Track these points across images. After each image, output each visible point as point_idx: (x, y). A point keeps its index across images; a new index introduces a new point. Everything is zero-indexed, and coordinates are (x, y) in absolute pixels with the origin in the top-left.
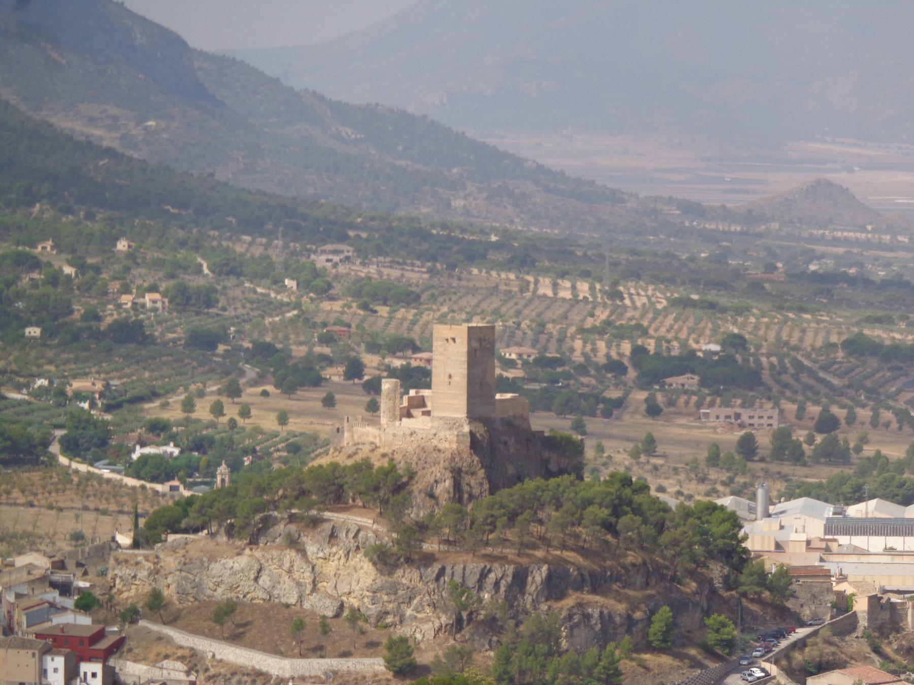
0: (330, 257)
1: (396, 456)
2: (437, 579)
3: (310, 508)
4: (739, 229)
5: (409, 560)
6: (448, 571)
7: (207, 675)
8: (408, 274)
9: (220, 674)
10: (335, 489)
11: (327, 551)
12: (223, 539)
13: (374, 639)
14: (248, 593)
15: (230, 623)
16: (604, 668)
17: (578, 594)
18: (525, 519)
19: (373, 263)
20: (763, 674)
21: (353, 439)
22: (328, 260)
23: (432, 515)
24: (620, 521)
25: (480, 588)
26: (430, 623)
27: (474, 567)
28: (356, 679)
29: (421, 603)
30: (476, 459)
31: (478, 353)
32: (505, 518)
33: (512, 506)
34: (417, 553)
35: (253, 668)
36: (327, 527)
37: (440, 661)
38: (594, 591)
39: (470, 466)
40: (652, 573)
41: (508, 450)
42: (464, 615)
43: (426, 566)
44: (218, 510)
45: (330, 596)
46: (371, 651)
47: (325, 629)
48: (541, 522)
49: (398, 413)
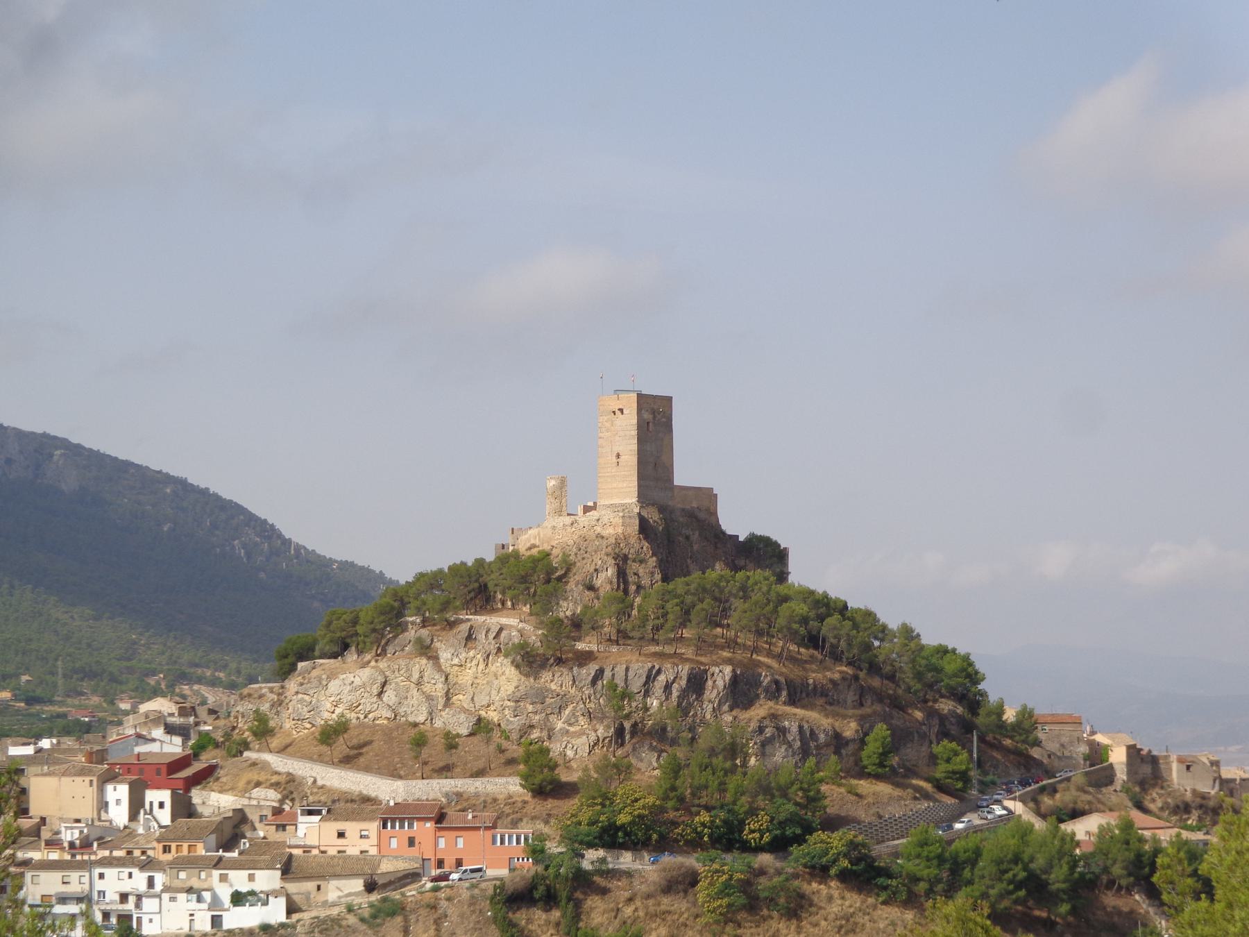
2: (594, 682)
5: (560, 661)
6: (608, 674)
14: (370, 712)
17: (771, 704)
20: (1005, 812)
25: (647, 694)
28: (485, 802)
35: (361, 793)
36: (464, 628)
38: (792, 701)
39: (638, 553)
43: (581, 665)
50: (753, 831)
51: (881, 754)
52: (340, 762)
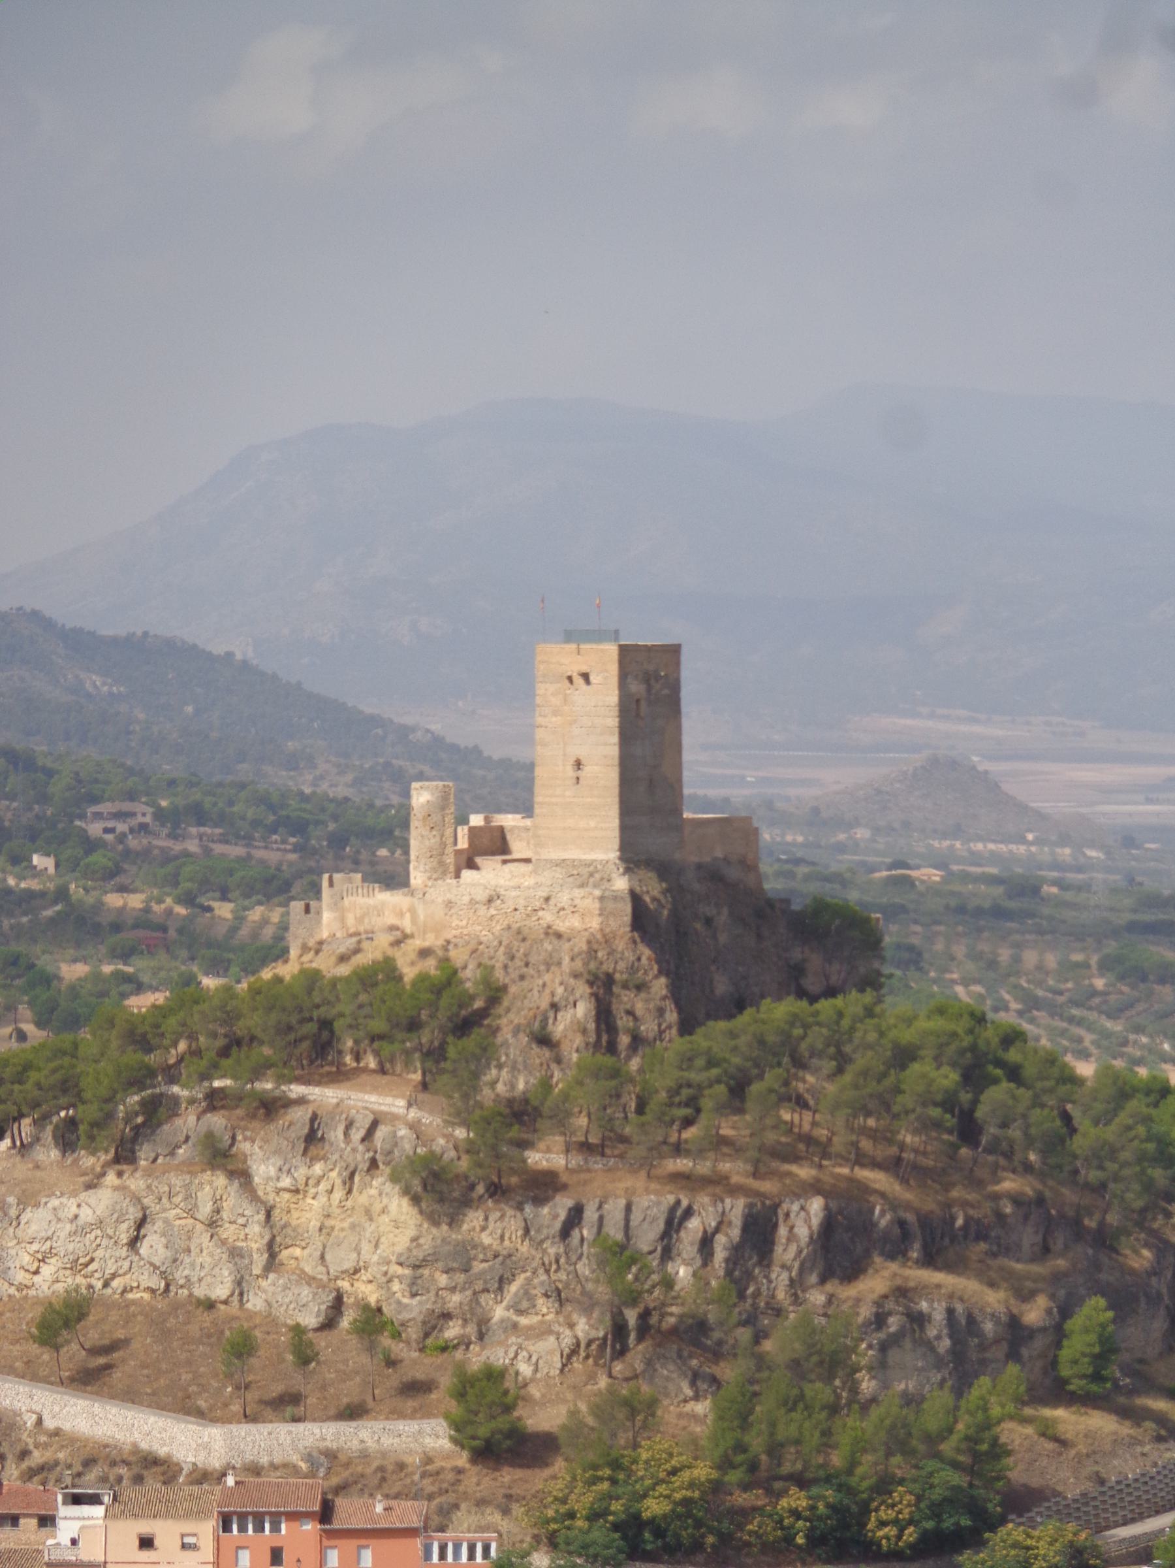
0: (110, 824)
1: (453, 954)
3: (257, 1073)
4: (800, 839)
5: (497, 1191)
6: (590, 1214)
7: (24, 1466)
8: (259, 854)
9: (57, 1463)
10: (315, 1032)
11: (301, 1173)
12: (48, 1154)
13: (420, 1375)
14: (114, 1276)
15: (74, 1346)
16: (967, 1438)
17: (894, 1267)
18: (771, 1091)
19: (191, 837)
21: (343, 925)
22: (107, 831)
23: (546, 1085)
24: (983, 1098)
25: (667, 1254)
26: (552, 1339)
27: (653, 1204)
28: (381, 1469)
29: (526, 1294)
30: (646, 952)
31: (643, 704)
32: (721, 1089)
33: (736, 1060)
34: (513, 1171)
35: (136, 1450)
36: (299, 1115)
37: (582, 1424)
38: (930, 1260)
39: (632, 969)
40: (1050, 1223)
41: (715, 937)
42: (631, 1316)
43: (539, 1201)
44: (39, 1086)
45: (311, 1280)
46: (410, 1404)
47: (304, 1353)
48: (801, 1103)
49: (450, 860)
50: (883, 1524)
51: (1096, 1357)
52: (72, 1380)
